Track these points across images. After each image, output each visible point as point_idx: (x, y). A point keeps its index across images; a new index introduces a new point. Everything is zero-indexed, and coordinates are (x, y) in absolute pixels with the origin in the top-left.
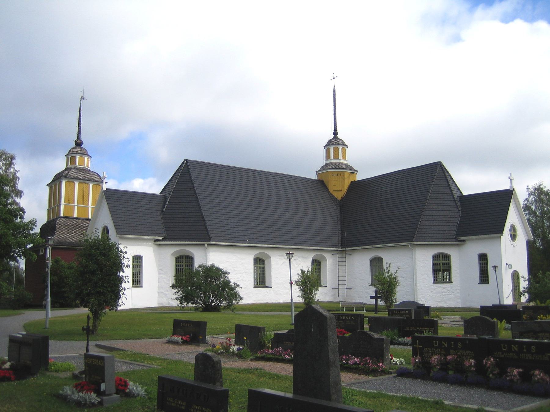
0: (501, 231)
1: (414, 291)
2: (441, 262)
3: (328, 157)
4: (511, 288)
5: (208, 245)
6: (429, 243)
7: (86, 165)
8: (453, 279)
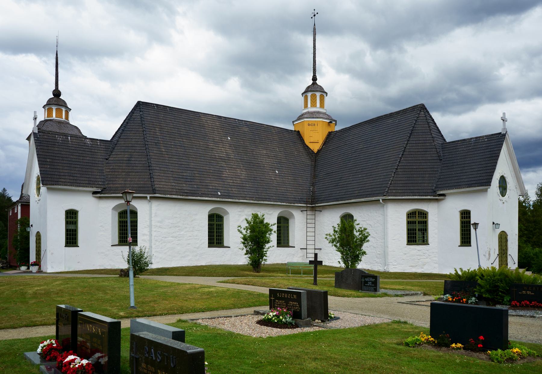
0: (488, 183)
1: (385, 255)
3: (306, 106)
4: (497, 252)
5: (151, 197)
6: (403, 197)
7: (64, 117)
8: (430, 240)
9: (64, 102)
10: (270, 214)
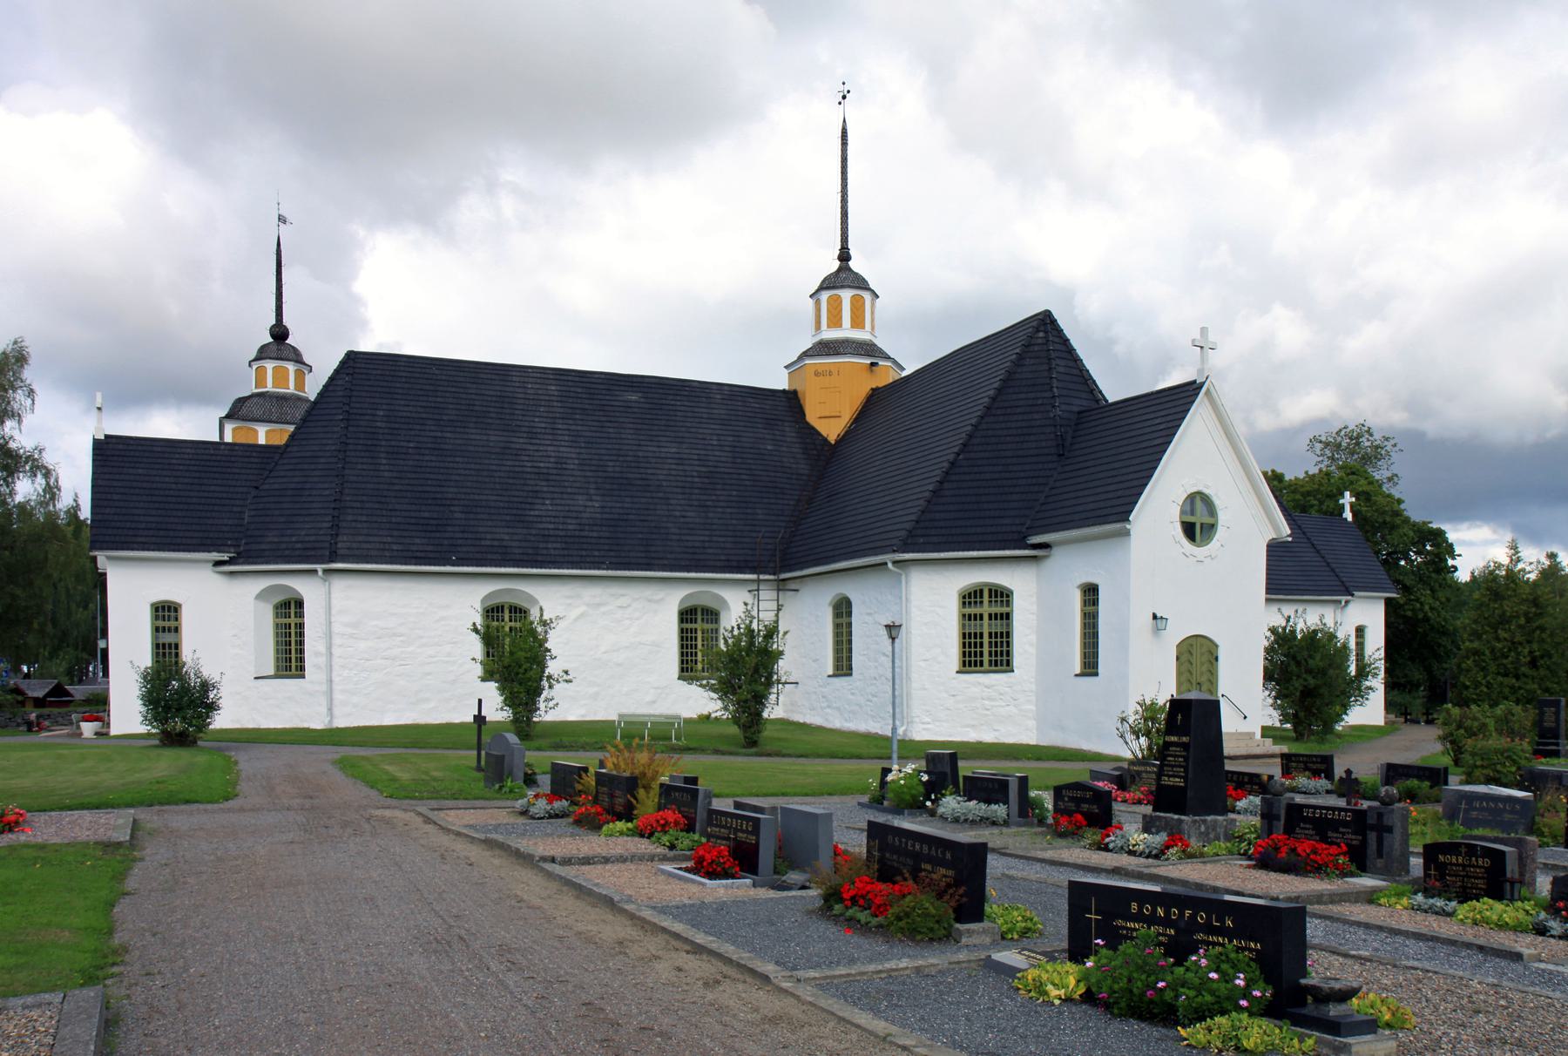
2: (986, 609)
8: (1018, 659)
9: (295, 350)
10: (658, 602)
